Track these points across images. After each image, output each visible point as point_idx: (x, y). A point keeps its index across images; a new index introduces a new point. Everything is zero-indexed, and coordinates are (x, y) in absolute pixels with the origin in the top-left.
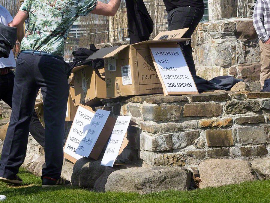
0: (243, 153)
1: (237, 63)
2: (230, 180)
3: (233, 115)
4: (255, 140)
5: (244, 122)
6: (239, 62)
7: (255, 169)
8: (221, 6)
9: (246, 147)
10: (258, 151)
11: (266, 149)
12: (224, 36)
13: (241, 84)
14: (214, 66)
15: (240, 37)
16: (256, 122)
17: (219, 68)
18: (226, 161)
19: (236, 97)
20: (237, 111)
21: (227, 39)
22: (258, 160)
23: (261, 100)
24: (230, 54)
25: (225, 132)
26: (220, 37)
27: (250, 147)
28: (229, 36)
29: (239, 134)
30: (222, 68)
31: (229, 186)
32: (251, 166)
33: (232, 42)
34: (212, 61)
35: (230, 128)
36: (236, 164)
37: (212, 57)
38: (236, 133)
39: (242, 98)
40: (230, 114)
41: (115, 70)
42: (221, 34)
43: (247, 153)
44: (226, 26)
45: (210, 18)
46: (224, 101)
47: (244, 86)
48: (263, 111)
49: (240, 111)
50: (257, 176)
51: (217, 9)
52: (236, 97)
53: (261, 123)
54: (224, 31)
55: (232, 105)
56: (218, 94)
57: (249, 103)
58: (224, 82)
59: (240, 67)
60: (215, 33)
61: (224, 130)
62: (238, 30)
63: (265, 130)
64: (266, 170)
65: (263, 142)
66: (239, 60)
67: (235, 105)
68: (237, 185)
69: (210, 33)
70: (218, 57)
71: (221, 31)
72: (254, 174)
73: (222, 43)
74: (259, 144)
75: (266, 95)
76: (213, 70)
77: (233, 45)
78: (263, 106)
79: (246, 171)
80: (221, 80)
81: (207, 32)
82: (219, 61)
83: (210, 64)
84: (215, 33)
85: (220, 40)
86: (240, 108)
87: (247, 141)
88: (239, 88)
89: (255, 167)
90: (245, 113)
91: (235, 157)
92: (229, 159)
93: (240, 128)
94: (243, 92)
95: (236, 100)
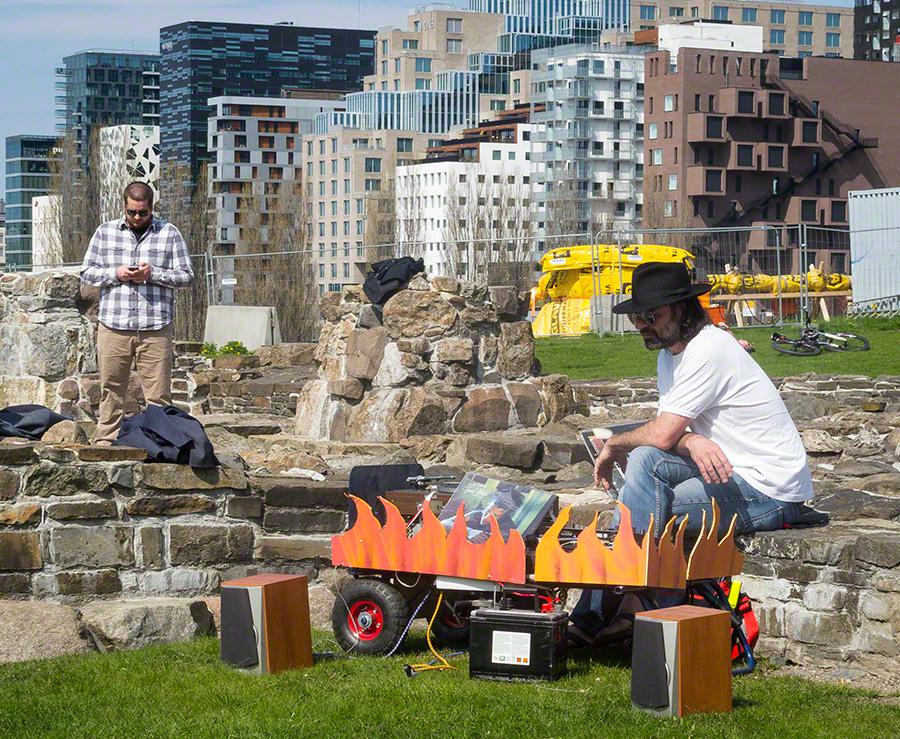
0: (64, 586)
1: (80, 371)
2: (30, 649)
3: (44, 499)
4: (93, 559)
5: (69, 515)
6: (84, 369)
7: (90, 625)
8: (61, 231)
9: (71, 572)
10: (98, 583)
11: (119, 580)
12: (49, 306)
13: (67, 426)
14: (25, 376)
15: (89, 311)
16: (96, 516)
17: (36, 382)
18: (22, 604)
19: (51, 457)
20: (52, 490)
21: (57, 314)
22: (98, 604)
23: (112, 465)
24: (62, 349)
25: (23, 538)
26: (42, 309)
27: (81, 575)
28: (62, 307)
29: (56, 542)
30: (43, 383)
31: (24, 664)
32: (79, 619)
33: (68, 322)
34: (21, 363)
35: (35, 528)
36: (45, 612)
37: (20, 355)
38: (49, 540)
39: (67, 459)
40: (37, 494)
41: (724, 193)
42: (44, 301)
43: (72, 587)
44: (57, 284)
45: (36, 260)
46: (23, 465)
47: (71, 431)
48: (115, 492)
49: (61, 489)
50: (93, 642)
51: (51, 238)
52: (51, 457)
53: (108, 518)
54: (51, 296)
55: (43, 475)
56: (9, 448)
57: (83, 472)
58: (27, 419)
59: (87, 381)
60: (30, 298)
61: (21, 531)
62: (84, 295)
63: (116, 536)
64: (115, 628)
65: (112, 563)
66: (84, 364)
67: (50, 476)
68: (42, 663)
69: (19, 298)
70: (36, 354)
71: (44, 295)
72: (86, 638)
73: (45, 323)
74: (101, 568)
75: (124, 455)
76: (21, 384)
77: (71, 328)
78: (115, 480)
79: (67, 631)
80: (22, 414)
81: (10, 296)
82: (36, 365)
83: (15, 371)
84: (30, 298)
85: (42, 316)
86: (60, 483)
87: (73, 559)
88: (60, 435)
89: (91, 620)
90: (72, 493)
91: (43, 596)
92: (29, 600)
93: (59, 529)
94: (70, 444)
95: (52, 464)
